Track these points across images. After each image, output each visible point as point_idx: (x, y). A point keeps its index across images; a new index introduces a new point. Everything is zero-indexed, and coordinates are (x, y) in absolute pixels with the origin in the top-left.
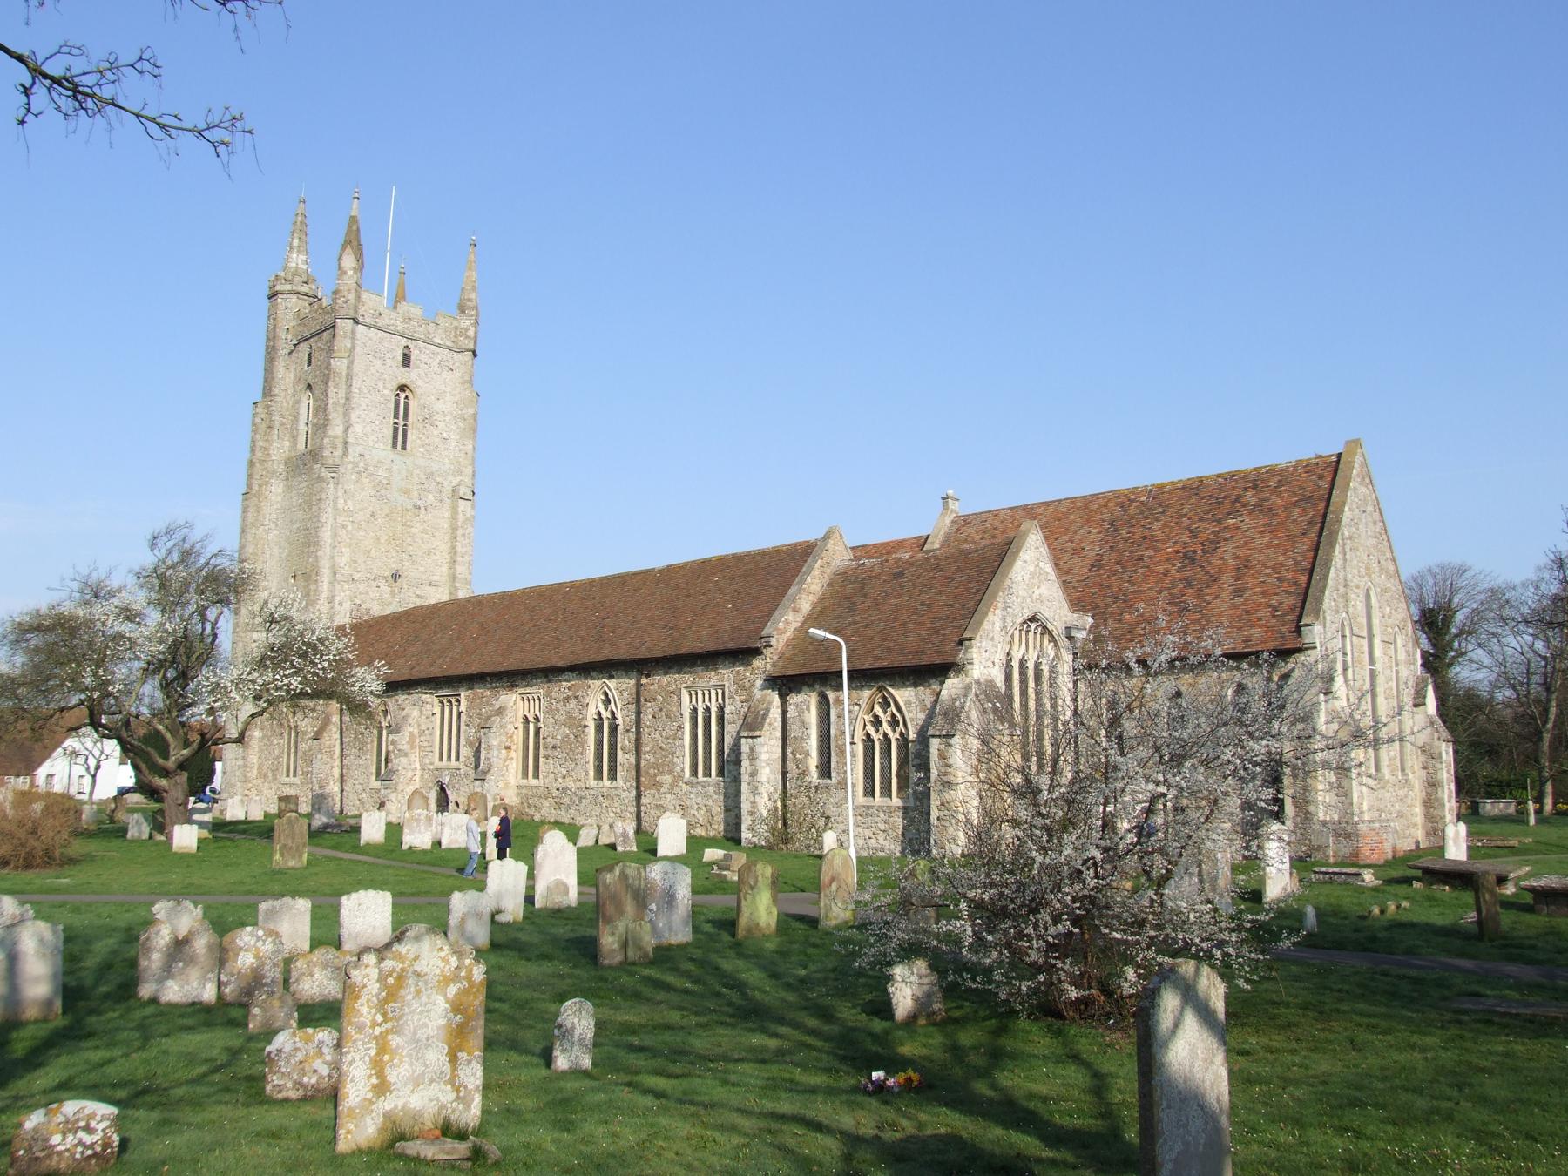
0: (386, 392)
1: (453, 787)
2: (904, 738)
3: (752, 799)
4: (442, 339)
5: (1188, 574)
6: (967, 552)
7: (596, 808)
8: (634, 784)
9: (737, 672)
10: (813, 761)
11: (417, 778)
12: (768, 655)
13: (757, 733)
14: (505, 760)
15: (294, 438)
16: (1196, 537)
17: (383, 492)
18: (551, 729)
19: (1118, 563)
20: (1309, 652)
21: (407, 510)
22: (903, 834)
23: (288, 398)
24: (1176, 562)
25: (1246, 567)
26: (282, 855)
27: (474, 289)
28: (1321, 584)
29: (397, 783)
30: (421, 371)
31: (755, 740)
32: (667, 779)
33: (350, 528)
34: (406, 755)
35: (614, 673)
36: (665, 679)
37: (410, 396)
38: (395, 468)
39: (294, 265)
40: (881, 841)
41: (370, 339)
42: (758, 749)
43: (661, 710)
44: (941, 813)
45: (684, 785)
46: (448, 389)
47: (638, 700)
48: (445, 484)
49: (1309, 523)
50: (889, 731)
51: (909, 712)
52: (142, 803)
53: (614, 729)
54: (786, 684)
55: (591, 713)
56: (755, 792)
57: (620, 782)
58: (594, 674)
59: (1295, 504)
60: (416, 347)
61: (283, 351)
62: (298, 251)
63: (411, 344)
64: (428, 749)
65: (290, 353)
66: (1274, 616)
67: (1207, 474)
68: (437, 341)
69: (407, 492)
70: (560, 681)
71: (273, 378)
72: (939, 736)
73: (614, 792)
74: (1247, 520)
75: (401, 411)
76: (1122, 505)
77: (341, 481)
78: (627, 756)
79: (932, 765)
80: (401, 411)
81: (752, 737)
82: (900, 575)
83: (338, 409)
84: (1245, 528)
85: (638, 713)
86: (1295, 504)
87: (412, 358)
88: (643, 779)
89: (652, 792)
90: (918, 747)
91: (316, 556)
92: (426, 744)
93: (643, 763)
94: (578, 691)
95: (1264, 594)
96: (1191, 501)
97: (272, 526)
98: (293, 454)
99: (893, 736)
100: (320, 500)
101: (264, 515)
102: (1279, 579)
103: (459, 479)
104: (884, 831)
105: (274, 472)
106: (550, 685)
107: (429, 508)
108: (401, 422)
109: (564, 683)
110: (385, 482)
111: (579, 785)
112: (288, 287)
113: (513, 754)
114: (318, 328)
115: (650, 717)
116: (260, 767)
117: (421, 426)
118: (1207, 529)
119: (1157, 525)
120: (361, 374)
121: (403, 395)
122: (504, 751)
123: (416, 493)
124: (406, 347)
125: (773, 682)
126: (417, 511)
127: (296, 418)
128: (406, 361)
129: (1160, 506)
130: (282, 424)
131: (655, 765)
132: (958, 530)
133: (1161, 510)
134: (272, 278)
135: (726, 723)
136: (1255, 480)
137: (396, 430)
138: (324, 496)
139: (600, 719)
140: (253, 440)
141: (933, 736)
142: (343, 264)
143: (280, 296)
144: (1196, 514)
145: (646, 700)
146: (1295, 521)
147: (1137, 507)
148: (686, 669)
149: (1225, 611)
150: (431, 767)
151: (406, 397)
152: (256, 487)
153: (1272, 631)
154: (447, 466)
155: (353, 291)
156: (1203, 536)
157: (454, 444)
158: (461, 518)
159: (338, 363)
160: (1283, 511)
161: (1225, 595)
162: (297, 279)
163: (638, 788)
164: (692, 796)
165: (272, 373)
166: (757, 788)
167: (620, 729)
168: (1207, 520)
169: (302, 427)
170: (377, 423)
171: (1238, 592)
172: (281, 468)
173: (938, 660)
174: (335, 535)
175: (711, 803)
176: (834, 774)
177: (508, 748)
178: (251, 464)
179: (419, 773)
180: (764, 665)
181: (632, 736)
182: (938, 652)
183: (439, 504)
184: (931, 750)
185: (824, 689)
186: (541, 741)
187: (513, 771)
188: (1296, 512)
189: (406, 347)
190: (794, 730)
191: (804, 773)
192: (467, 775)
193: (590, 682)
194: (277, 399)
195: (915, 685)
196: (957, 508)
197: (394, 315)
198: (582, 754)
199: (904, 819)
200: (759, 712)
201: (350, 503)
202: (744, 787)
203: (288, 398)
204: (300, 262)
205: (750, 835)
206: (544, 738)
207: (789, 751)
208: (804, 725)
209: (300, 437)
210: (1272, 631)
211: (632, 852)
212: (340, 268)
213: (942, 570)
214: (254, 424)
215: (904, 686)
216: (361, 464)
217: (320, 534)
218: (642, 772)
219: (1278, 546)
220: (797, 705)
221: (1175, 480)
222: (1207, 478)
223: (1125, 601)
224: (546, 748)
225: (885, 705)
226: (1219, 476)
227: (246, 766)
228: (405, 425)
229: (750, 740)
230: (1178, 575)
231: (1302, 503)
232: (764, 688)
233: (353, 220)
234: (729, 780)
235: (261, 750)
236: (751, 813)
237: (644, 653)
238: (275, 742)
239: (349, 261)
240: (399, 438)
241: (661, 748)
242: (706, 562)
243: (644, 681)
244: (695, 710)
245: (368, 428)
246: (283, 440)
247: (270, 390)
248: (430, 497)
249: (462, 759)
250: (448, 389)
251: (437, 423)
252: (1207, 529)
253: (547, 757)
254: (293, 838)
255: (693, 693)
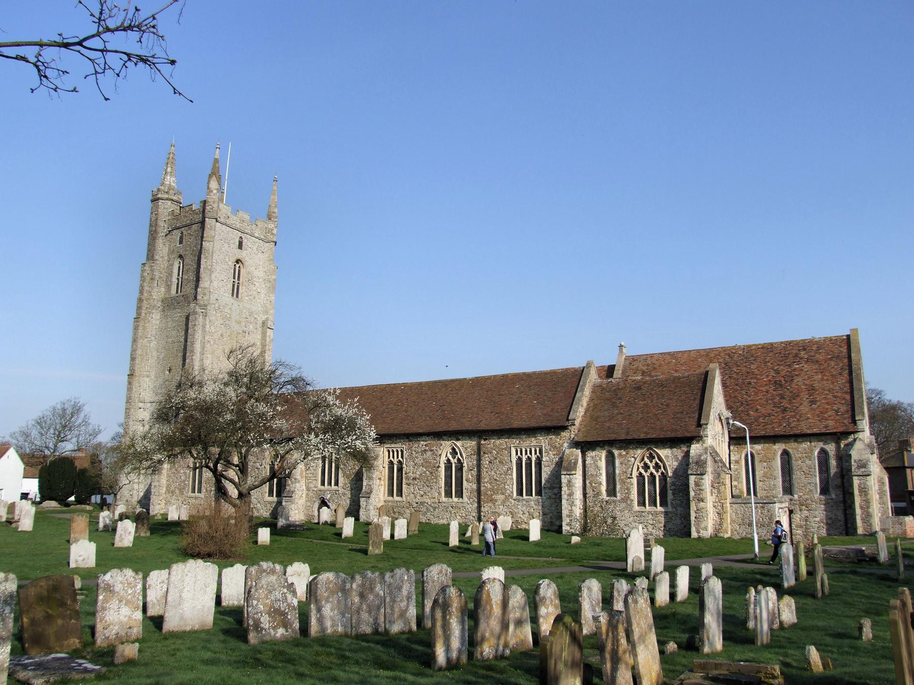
0: (230, 263)
1: (333, 501)
2: (664, 477)
3: (570, 508)
4: (259, 234)
5: (781, 392)
6: (679, 378)
7: (446, 513)
8: (476, 500)
9: (551, 438)
10: (604, 488)
11: (304, 495)
12: (572, 430)
13: (573, 472)
14: (379, 486)
15: (169, 287)
16: (778, 373)
17: (227, 322)
18: (412, 468)
19: (737, 385)
20: (861, 433)
21: (239, 333)
22: (665, 526)
23: (164, 262)
24: (771, 386)
25: (813, 390)
26: (373, 547)
27: (276, 207)
28: (860, 400)
29: (294, 499)
30: (247, 252)
31: (571, 476)
32: (500, 497)
33: (212, 343)
34: (299, 482)
35: (460, 437)
36: (498, 442)
37: (242, 266)
38: (234, 308)
39: (168, 183)
40: (650, 529)
41: (223, 231)
42: (573, 481)
43: (496, 459)
44: (697, 515)
45: (513, 501)
46: (261, 264)
47: (479, 453)
48: (259, 319)
49: (842, 369)
50: (654, 471)
51: (667, 461)
52: (57, 507)
53: (460, 468)
54: (585, 446)
55: (443, 459)
56: (572, 504)
57: (465, 499)
58: (445, 438)
59: (831, 359)
60: (246, 238)
61: (162, 232)
62: (171, 175)
63: (243, 236)
64: (313, 479)
65: (166, 235)
66: (837, 415)
67: (775, 341)
68: (256, 235)
69: (239, 323)
70: (419, 441)
71: (155, 250)
72: (695, 475)
73: (460, 505)
74: (806, 366)
75: (237, 275)
76: (729, 355)
77: (208, 314)
78: (471, 484)
79: (691, 489)
80: (237, 275)
81: (569, 475)
82: (639, 388)
83: (207, 271)
84: (806, 370)
85: (479, 460)
86: (831, 359)
87: (243, 244)
88: (482, 497)
89: (489, 504)
90: (674, 480)
91: (192, 359)
92: (311, 475)
93: (482, 489)
94: (433, 447)
95: (828, 403)
96: (769, 355)
97: (153, 338)
98: (167, 296)
99: (657, 475)
100: (195, 325)
101: (148, 332)
102: (834, 397)
103: (266, 316)
104: (652, 525)
105: (155, 306)
106: (411, 443)
107: (250, 333)
108: (237, 282)
109: (422, 443)
110: (228, 316)
111: (433, 500)
112: (166, 196)
113: (382, 482)
114: (188, 222)
115: (487, 462)
116: (168, 486)
117: (246, 284)
118: (783, 370)
119: (753, 367)
120: (218, 252)
121: (238, 266)
122: (378, 481)
123: (243, 324)
124: (241, 237)
125: (576, 444)
126: (244, 334)
127: (170, 274)
128: (240, 246)
129: (752, 356)
130: (160, 278)
131: (492, 490)
132: (630, 364)
133: (753, 358)
134: (155, 190)
135: (543, 466)
136: (805, 346)
137: (234, 285)
138: (197, 323)
139: (448, 464)
140: (142, 286)
141: (691, 474)
142: (211, 186)
143: (161, 201)
144: (775, 362)
145: (484, 453)
146: (833, 368)
147: (738, 357)
148: (513, 436)
149: (808, 412)
150: (316, 489)
151: (239, 267)
152: (143, 315)
153: (839, 422)
154: (260, 308)
155: (216, 203)
156: (783, 373)
157: (263, 296)
158: (268, 339)
159: (207, 244)
160: (825, 362)
161: (806, 403)
162: (171, 192)
163: (479, 502)
164: (519, 507)
165: (155, 247)
166: (573, 502)
167: (465, 469)
168: (782, 365)
169: (175, 280)
170: (225, 281)
171: (813, 402)
172: (159, 304)
173: (688, 435)
174: (203, 348)
175: (532, 510)
176: (618, 495)
177: (380, 479)
178: (140, 300)
179: (305, 492)
180: (572, 433)
181: (474, 473)
182: (687, 431)
183: (255, 331)
184: (690, 482)
185: (610, 449)
186: (404, 476)
187: (382, 492)
188: (832, 363)
189: (241, 237)
190: (591, 471)
191: (599, 494)
192: (344, 494)
193: (442, 442)
194: (158, 262)
195: (671, 447)
196: (628, 352)
197: (235, 218)
198: (436, 483)
199: (665, 518)
200: (571, 461)
201: (212, 328)
202: (564, 502)
203: (164, 262)
204: (171, 181)
205: (569, 528)
206: (406, 473)
207: (587, 482)
208: (598, 468)
209: (173, 286)
210: (839, 422)
211: (501, 539)
212: (208, 188)
213: (666, 386)
214: (142, 276)
215: (664, 447)
216: (217, 305)
217: (195, 346)
218: (482, 493)
219: (827, 380)
220: (592, 457)
221: (757, 343)
222: (776, 343)
223: (747, 405)
224: (407, 478)
225: (651, 457)
226: (782, 343)
227: (160, 486)
228: (238, 283)
229: (568, 476)
230: (774, 393)
231: (834, 359)
232: (570, 447)
233: (216, 161)
234: (545, 498)
235: (168, 476)
236: (569, 516)
237: (483, 426)
238: (182, 471)
239: (214, 185)
240: (235, 291)
241: (496, 480)
242: (505, 377)
243: (483, 442)
244: (520, 459)
245: (221, 284)
246: (160, 287)
247: (153, 256)
248: (251, 326)
249: (340, 484)
250: (261, 264)
251: (255, 283)
252: (784, 370)
253: (408, 484)
254: (377, 536)
255: (519, 450)
